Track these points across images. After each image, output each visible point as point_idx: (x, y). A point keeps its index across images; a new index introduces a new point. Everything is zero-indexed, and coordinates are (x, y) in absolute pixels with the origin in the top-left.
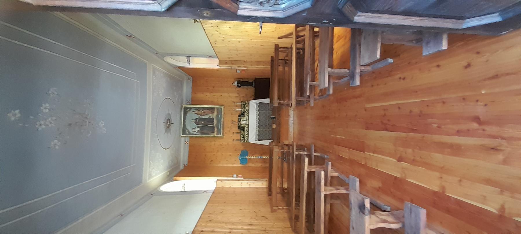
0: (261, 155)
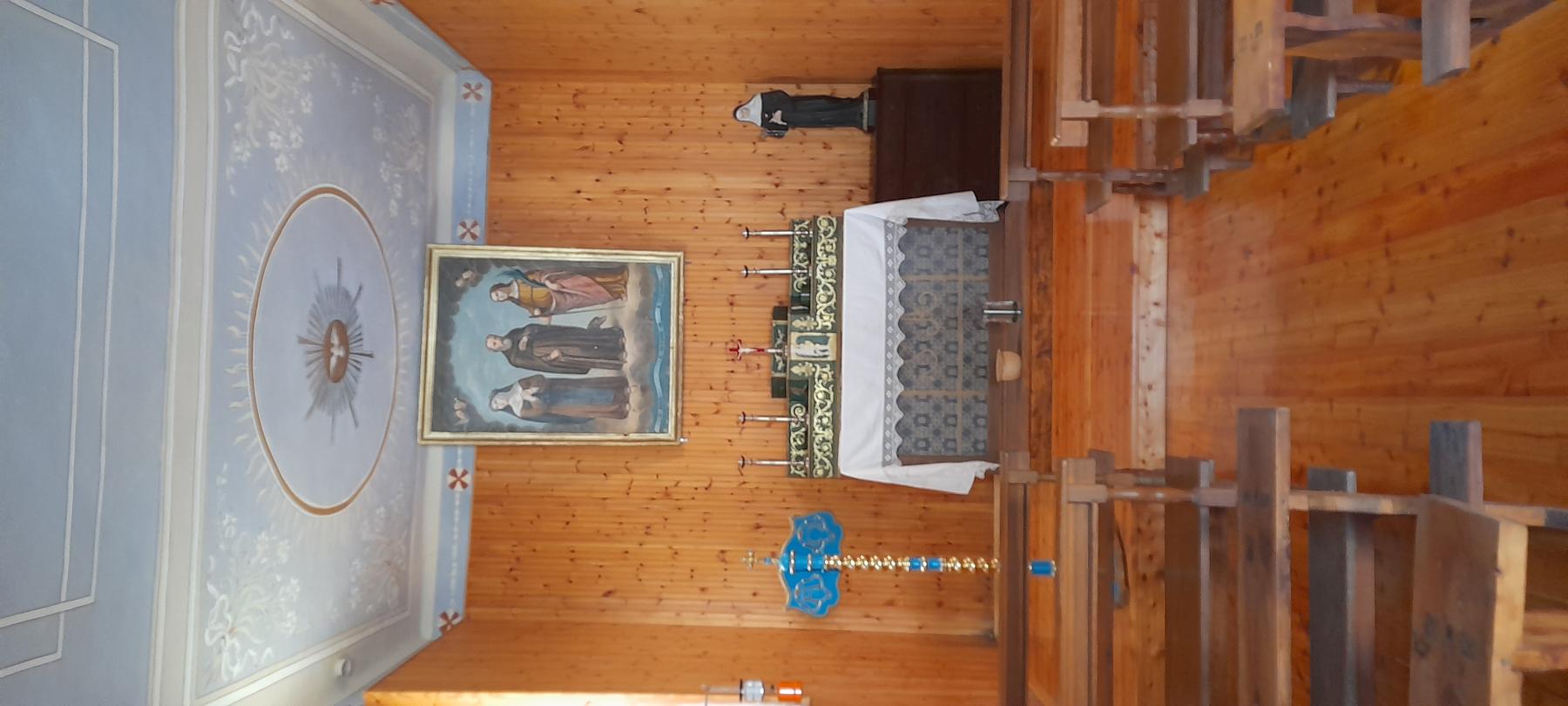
0: (933, 551)
